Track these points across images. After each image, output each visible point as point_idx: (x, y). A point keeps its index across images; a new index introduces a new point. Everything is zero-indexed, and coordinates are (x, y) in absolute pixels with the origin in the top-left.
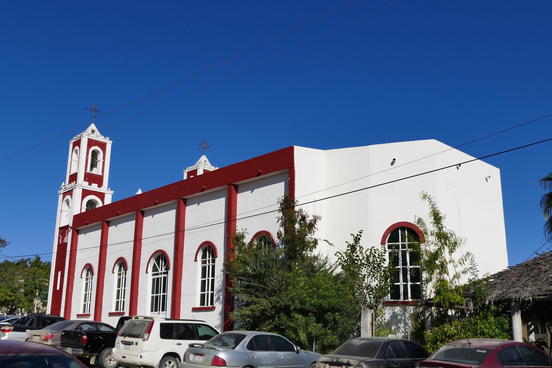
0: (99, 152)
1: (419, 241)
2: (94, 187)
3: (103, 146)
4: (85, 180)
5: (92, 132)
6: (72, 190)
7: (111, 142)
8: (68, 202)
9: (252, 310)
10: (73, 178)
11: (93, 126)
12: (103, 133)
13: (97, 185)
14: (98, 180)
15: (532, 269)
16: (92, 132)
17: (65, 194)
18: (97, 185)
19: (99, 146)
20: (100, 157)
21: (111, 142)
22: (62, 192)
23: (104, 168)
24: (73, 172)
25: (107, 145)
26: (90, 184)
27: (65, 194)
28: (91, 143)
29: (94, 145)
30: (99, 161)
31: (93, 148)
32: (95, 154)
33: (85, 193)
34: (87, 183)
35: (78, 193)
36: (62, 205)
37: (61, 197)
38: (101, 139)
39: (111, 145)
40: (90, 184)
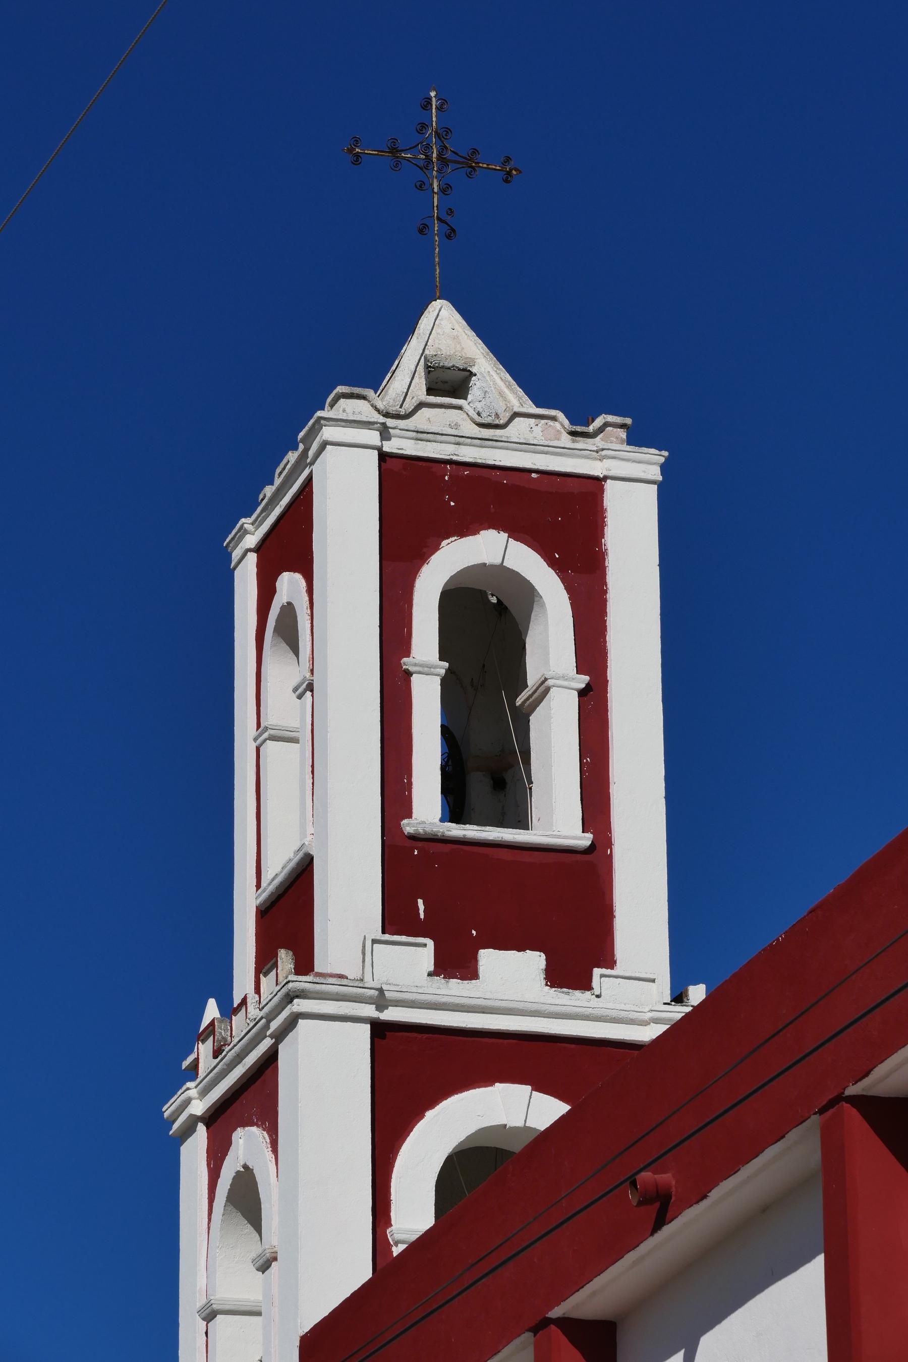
0: (528, 593)
1: (384, 457)
2: (511, 986)
3: (564, 520)
4: (397, 919)
5: (454, 388)
6: (270, 1060)
7: (649, 463)
8: (246, 1200)
9: (244, 1002)
10: (290, 916)
11: (443, 330)
12: (557, 382)
13: (536, 961)
14: (562, 908)
15: (597, 452)
16: (454, 388)
17: (221, 1120)
18: (536, 961)
19: (517, 532)
20: (551, 645)
21: (649, 463)
22: (198, 1108)
23: (606, 766)
24: (278, 864)
25: (614, 498)
26: (455, 963)
27: (221, 1120)
28: (422, 503)
29: (466, 529)
30: (543, 691)
31: (454, 558)
32: (485, 625)
33: (412, 1068)
34: (423, 954)
35: (328, 1075)
36: (209, 1260)
37: (194, 1151)
38: (539, 443)
39: (649, 496)
40: (455, 963)
